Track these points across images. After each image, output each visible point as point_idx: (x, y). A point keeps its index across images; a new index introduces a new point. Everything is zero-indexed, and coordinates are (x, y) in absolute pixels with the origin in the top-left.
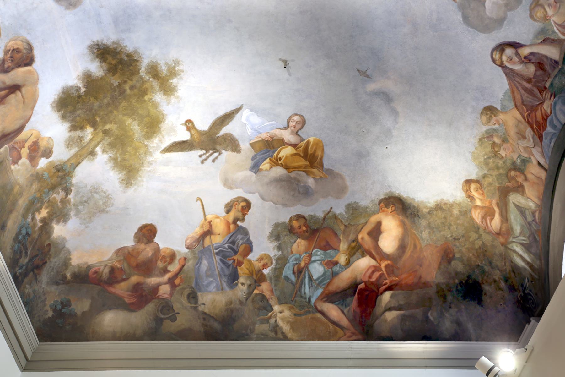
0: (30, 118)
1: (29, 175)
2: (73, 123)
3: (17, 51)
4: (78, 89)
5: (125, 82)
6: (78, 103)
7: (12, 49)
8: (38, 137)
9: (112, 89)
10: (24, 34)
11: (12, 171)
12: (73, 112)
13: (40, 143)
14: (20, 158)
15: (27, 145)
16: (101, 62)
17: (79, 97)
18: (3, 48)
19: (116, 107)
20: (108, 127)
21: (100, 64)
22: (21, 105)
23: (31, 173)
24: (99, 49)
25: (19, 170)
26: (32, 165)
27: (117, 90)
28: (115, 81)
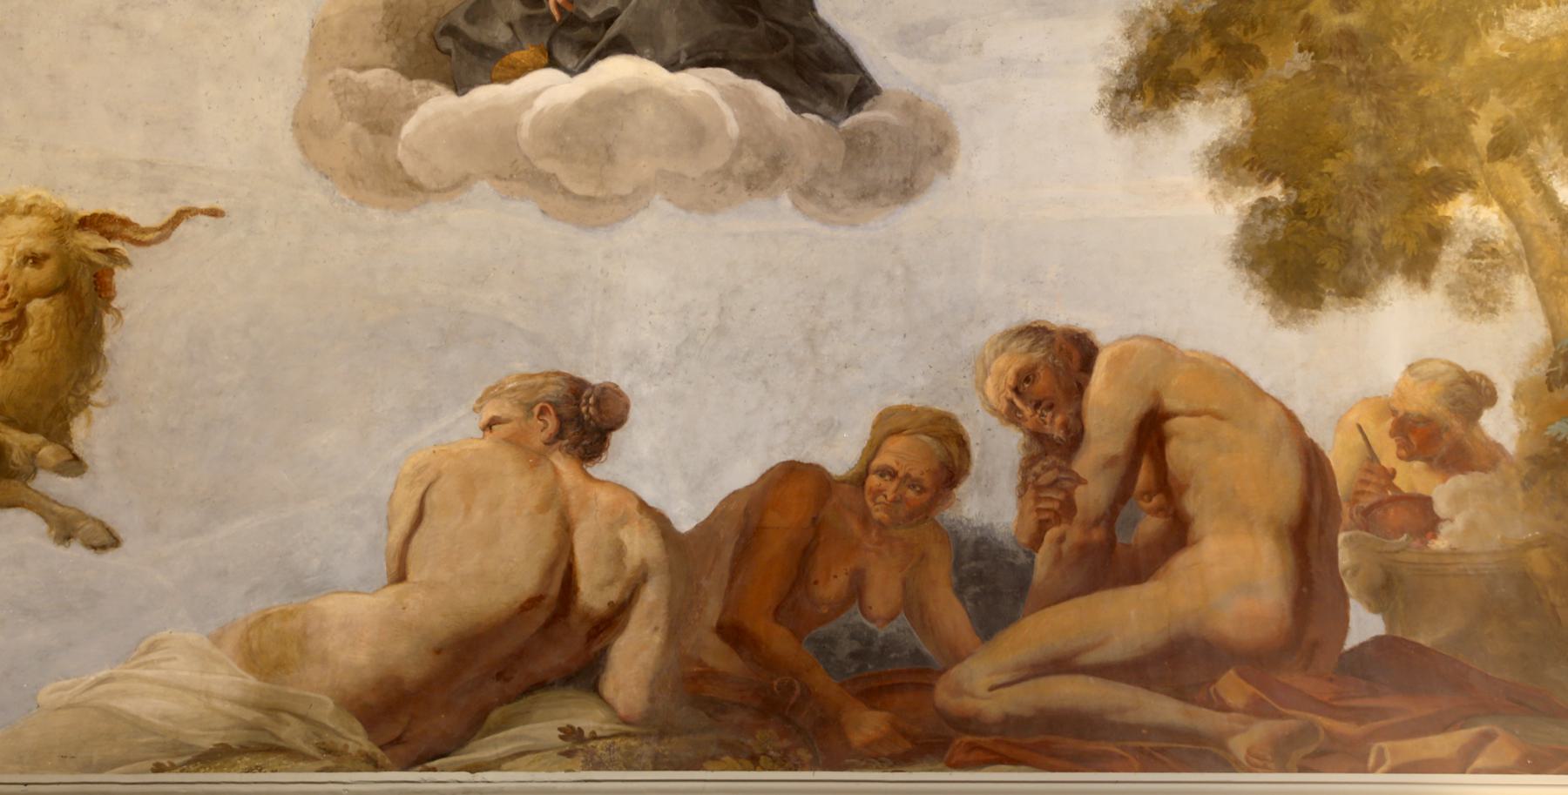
0: (1290, 415)
1: (1520, 495)
2: (1399, 262)
3: (1025, 378)
4: (1265, 209)
5: (1308, 23)
6: (1321, 223)
7: (1010, 394)
8: (1386, 408)
9: (1318, 82)
10: (980, 337)
11: (1453, 552)
12: (1348, 249)
13: (1413, 408)
14: (1425, 503)
15: (1389, 456)
16: (1190, 99)
17: (1298, 210)
18: (994, 421)
19: (1408, 81)
20: (1482, 133)
21: (1197, 104)
22: (1225, 430)
23: (1516, 484)
24: (1134, 93)
25: (1471, 526)
26: (1484, 470)
27: (1330, 61)
28: (1288, 62)
